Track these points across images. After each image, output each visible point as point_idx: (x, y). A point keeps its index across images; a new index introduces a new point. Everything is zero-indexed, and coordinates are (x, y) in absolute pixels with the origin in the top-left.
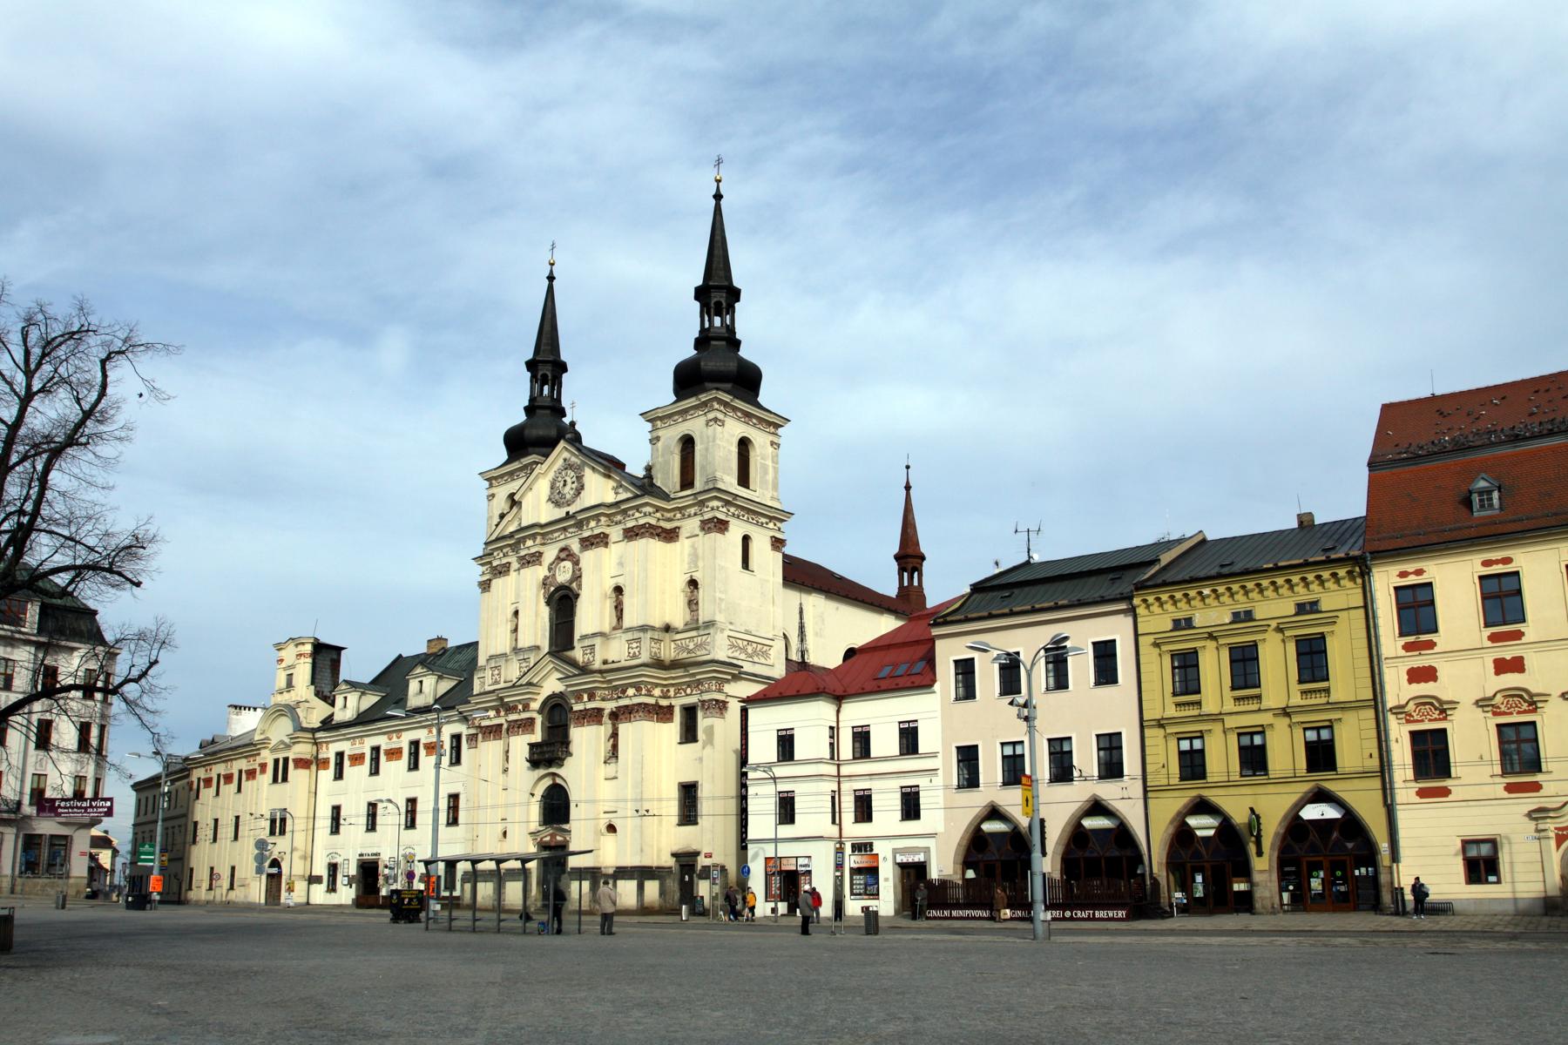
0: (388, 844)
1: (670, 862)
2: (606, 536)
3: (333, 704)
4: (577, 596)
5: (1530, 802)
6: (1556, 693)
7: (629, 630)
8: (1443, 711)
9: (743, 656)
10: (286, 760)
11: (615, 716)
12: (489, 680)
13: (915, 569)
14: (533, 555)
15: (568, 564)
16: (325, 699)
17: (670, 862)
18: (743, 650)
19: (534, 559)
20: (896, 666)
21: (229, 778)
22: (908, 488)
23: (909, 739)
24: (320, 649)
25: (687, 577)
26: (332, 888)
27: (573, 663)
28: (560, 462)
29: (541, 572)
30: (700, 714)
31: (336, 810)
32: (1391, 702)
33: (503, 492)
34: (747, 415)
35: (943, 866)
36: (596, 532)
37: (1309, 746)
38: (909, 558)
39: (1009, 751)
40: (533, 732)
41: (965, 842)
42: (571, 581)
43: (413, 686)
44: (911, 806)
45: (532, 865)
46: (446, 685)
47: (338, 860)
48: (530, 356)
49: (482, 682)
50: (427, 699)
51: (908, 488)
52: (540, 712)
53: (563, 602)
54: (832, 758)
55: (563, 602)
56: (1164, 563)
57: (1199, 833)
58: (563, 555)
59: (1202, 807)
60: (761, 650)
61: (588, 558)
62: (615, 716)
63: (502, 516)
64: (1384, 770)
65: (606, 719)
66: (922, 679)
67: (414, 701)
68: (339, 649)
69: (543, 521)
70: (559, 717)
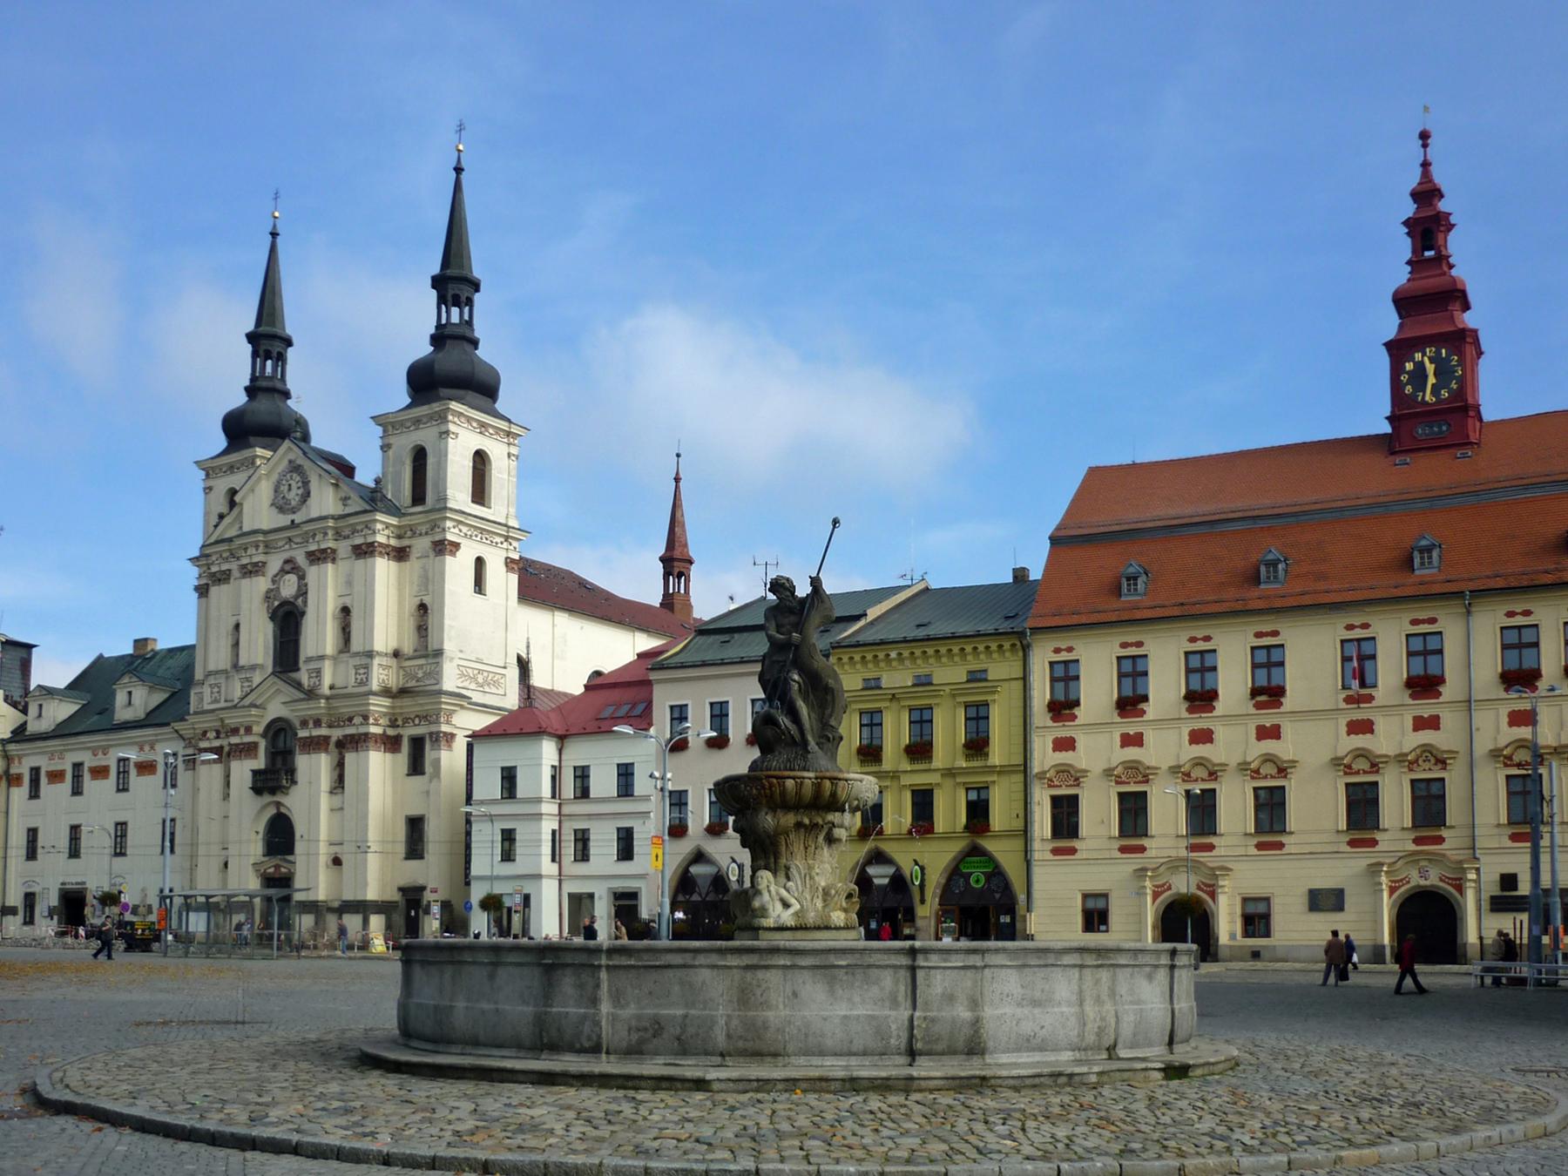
0: (93, 874)
1: (396, 897)
3: (25, 711)
4: (303, 614)
5: (1135, 861)
6: (1165, 767)
7: (357, 654)
8: (1077, 779)
9: (473, 686)
11: (342, 745)
12: (207, 698)
13: (680, 575)
14: (256, 564)
16: (14, 705)
17: (396, 897)
18: (474, 679)
20: (634, 706)
22: (677, 480)
23: (626, 774)
25: (417, 601)
26: (29, 920)
27: (298, 685)
28: (285, 463)
29: (262, 584)
31: (33, 834)
32: (1036, 768)
33: (222, 484)
34: (483, 425)
35: (654, 904)
36: (255, 560)
37: (970, 804)
38: (675, 563)
39: (973, 796)
40: (256, 757)
42: (296, 597)
43: (121, 698)
44: (626, 850)
45: (257, 901)
46: (158, 698)
47: (36, 889)
49: (202, 698)
50: (138, 711)
51: (677, 480)
52: (264, 735)
53: (288, 620)
54: (553, 797)
56: (870, 618)
57: (876, 881)
59: (878, 857)
60: (492, 681)
61: (312, 572)
62: (342, 745)
63: (221, 517)
64: (1025, 833)
65: (332, 746)
66: (642, 719)
67: (122, 714)
69: (265, 527)
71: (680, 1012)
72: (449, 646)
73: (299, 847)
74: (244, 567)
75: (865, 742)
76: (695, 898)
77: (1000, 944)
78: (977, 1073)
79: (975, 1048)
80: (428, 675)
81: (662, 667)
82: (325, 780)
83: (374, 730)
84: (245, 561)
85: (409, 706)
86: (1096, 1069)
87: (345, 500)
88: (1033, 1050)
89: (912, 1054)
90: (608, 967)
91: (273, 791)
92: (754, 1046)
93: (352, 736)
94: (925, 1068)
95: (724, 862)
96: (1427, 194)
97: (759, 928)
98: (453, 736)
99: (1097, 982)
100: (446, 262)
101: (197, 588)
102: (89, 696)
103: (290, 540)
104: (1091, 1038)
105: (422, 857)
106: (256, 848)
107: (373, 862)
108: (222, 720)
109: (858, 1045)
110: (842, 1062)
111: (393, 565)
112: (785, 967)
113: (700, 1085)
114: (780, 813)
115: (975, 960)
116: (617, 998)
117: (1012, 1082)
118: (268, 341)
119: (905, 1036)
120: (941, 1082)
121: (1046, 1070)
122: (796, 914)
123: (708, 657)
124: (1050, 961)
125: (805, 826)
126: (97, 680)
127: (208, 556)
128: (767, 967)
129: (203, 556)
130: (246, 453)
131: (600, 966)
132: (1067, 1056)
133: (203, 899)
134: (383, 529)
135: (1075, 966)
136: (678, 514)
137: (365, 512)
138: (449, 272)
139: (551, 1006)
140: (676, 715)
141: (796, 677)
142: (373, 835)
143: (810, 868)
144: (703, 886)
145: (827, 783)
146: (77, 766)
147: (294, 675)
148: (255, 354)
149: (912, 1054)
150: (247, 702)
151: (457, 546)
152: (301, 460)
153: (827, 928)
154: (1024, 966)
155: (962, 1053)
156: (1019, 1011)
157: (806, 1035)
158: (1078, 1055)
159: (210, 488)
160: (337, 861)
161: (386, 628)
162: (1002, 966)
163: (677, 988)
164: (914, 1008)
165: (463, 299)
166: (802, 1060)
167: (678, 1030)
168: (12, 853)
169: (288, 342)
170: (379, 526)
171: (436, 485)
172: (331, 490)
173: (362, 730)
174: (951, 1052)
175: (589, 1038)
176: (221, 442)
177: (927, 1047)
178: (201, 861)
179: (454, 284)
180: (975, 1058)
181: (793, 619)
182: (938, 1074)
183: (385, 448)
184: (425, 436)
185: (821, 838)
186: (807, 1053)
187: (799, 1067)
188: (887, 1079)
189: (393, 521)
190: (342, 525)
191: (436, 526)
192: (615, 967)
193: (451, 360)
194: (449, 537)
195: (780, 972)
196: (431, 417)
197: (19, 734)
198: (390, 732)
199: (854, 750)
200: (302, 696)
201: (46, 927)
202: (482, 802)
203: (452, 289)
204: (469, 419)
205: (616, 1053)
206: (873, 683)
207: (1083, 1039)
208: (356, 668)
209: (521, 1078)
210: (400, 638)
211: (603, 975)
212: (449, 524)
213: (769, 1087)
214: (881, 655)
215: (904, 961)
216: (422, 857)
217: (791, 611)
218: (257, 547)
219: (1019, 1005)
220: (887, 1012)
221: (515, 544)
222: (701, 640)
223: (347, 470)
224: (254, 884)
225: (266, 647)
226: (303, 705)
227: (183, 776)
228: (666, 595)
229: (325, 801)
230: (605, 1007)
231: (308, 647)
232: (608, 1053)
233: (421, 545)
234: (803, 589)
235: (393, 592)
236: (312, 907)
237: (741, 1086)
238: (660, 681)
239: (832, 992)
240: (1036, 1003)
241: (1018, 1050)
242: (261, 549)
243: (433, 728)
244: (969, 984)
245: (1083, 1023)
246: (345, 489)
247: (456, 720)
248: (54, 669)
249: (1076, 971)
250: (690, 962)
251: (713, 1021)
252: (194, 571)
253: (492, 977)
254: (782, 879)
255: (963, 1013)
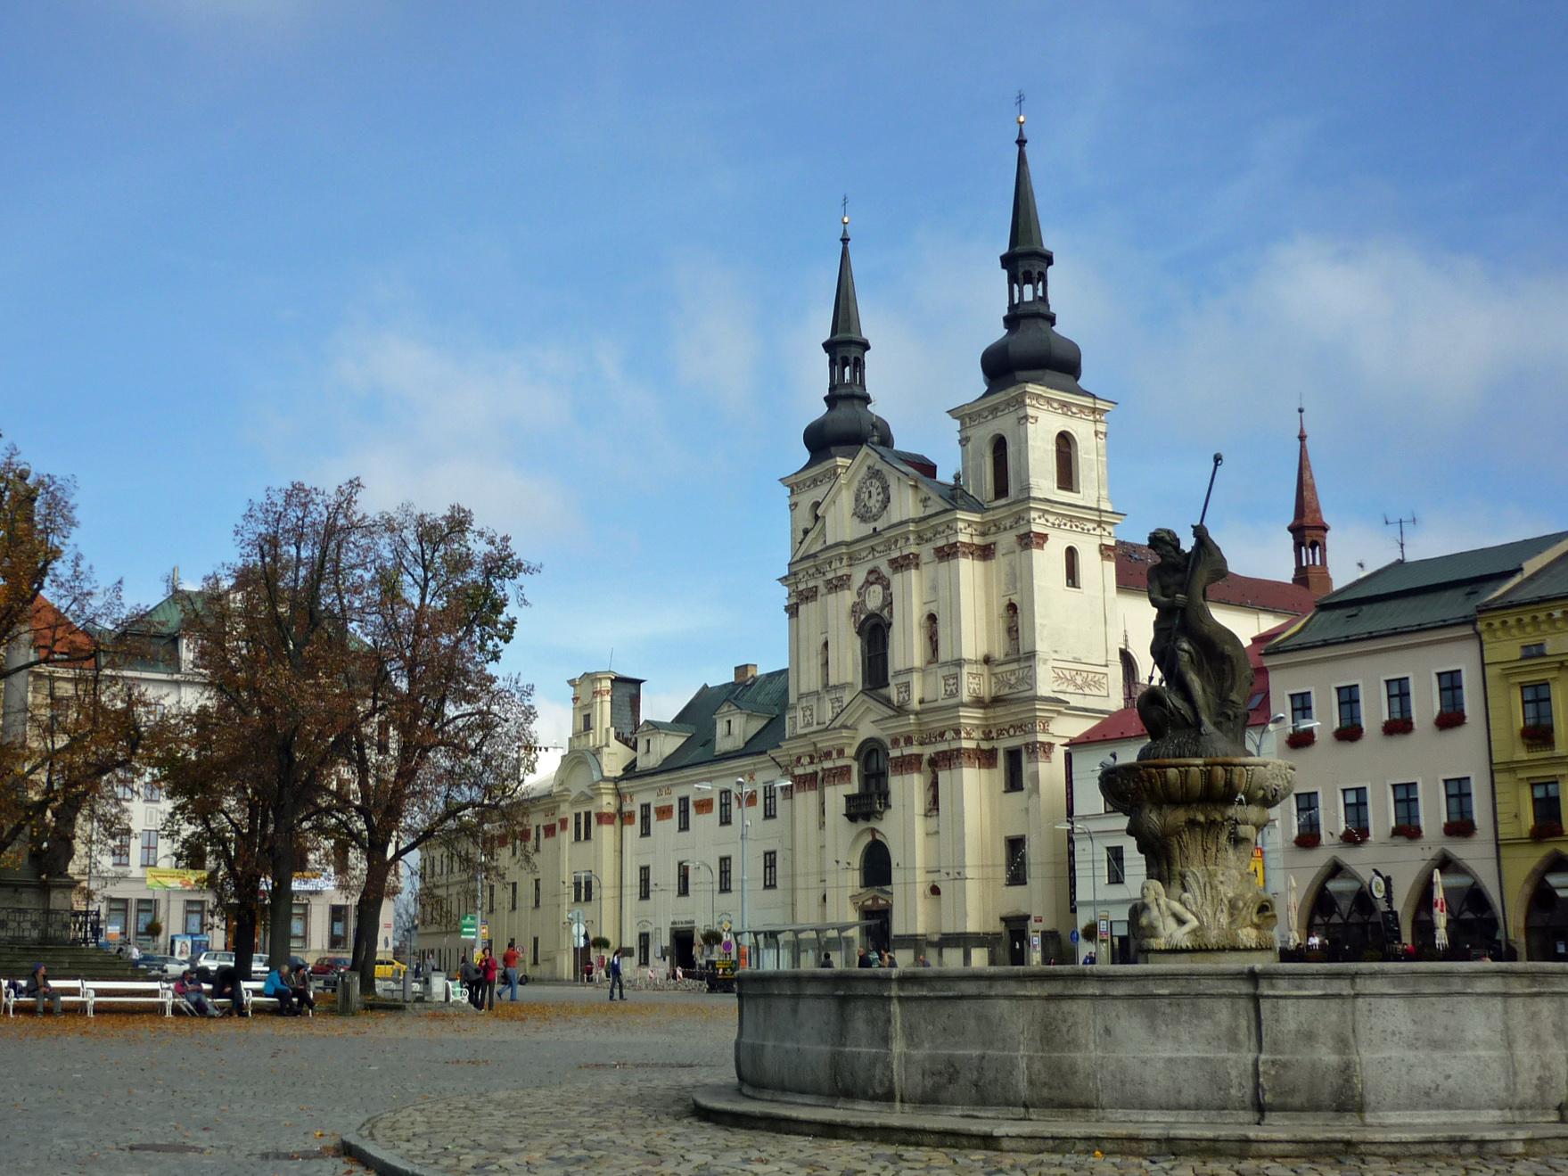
0: (701, 912)
1: (999, 927)
2: (917, 556)
3: (635, 748)
4: (890, 624)
7: (945, 664)
10: (588, 815)
12: (800, 722)
13: (1313, 545)
14: (840, 578)
15: (878, 588)
16: (625, 742)
17: (999, 927)
18: (1072, 681)
19: (838, 584)
21: (704, 806)
22: (1302, 438)
24: (618, 681)
26: (644, 962)
27: (887, 702)
29: (848, 598)
30: (1024, 758)
31: (645, 871)
33: (806, 499)
34: (1064, 405)
38: (1307, 532)
39: (1540, 793)
40: (849, 781)
41: (1308, 904)
42: (882, 609)
43: (721, 728)
46: (756, 725)
47: (650, 929)
48: (827, 336)
49: (796, 722)
50: (736, 742)
51: (1302, 438)
52: (856, 758)
53: (875, 632)
55: (875, 632)
58: (872, 578)
60: (1094, 682)
61: (897, 580)
63: (806, 532)
67: (723, 744)
68: (638, 682)
69: (848, 539)
70: (876, 766)
71: (975, 1052)
72: (1041, 647)
73: (896, 875)
74: (830, 581)
75: (1531, 722)
76: (1336, 919)
77: (1376, 966)
78: (1338, 1135)
79: (1348, 1102)
80: (1020, 680)
81: (1277, 651)
82: (919, 802)
83: (966, 744)
84: (830, 576)
85: (1002, 715)
86: (1520, 1135)
87: (925, 501)
88: (1438, 1107)
89: (1260, 1108)
90: (900, 998)
91: (867, 817)
92: (1062, 1097)
93: (944, 752)
94: (1279, 1128)
95: (1366, 875)
96: (1302, 430)
97: (1149, 951)
98: (1051, 745)
99: (1534, 1016)
100: (1014, 241)
101: (787, 609)
102: (694, 729)
103: (873, 549)
104: (1527, 1093)
105: (1025, 883)
106: (854, 879)
107: (972, 890)
108: (815, 744)
109: (1188, 1096)
110: (1168, 1117)
111: (978, 564)
112: (1093, 996)
113: (988, 1142)
114: (1166, 810)
115: (1343, 987)
116: (911, 1036)
117: (1390, 1149)
118: (846, 349)
119: (1249, 1085)
120: (1289, 1147)
121: (1440, 1135)
122: (1194, 931)
123: (1329, 635)
124: (1455, 988)
125: (1199, 824)
126: (699, 714)
127: (795, 574)
128: (1073, 997)
129: (793, 574)
130: (828, 464)
131: (890, 998)
132: (1493, 1115)
133: (813, 935)
134: (966, 527)
135: (1494, 994)
136: (1306, 476)
137: (946, 511)
138: (1018, 249)
139: (844, 1045)
140: (1298, 705)
141: (1185, 646)
142: (971, 858)
143: (1211, 875)
144: (1344, 905)
145: (1219, 771)
146: (646, 807)
147: (883, 691)
148: (832, 363)
149: (1260, 1108)
150: (837, 723)
151: (1044, 537)
152: (880, 465)
153: (1235, 949)
154: (1415, 995)
155: (1328, 1109)
156: (1410, 1055)
157: (1123, 1083)
158: (1508, 1115)
159: (796, 504)
160: (935, 891)
161: (974, 634)
162: (1382, 995)
163: (972, 1023)
164: (1260, 1049)
165: (1035, 275)
166: (1119, 1114)
167: (975, 1076)
168: (627, 891)
169: (865, 346)
170: (961, 525)
171: (1018, 474)
172: (910, 492)
173: (954, 745)
174: (1315, 1107)
175: (881, 1083)
176: (805, 456)
177: (1278, 1101)
178: (800, 895)
179: (1025, 261)
180: (1348, 1116)
181: (1178, 577)
182: (1283, 1136)
183: (964, 441)
184: (1004, 424)
185: (1223, 839)
186: (1126, 1104)
187: (1116, 1123)
188: (1215, 1140)
189: (976, 518)
190: (924, 527)
191: (1020, 518)
192: (908, 999)
193: (1029, 338)
194: (1035, 528)
195: (1089, 1003)
196: (1008, 404)
197: (630, 771)
198: (985, 746)
199: (1517, 733)
200: (892, 713)
201: (660, 968)
202: (1084, 818)
203: (1023, 267)
204: (1049, 401)
205: (911, 1101)
206: (1534, 650)
207: (1514, 1093)
208: (945, 678)
209: (805, 1128)
210: (990, 641)
211: (895, 1008)
212: (1034, 514)
213: (1068, 1146)
214: (1542, 616)
215: (1245, 988)
216: (1025, 883)
217: (1176, 568)
218: (841, 560)
219: (1411, 1046)
220: (1224, 1054)
221: (1109, 529)
222: (1323, 616)
223: (928, 469)
224: (853, 916)
225: (855, 665)
226: (891, 724)
227: (781, 805)
228: (1300, 569)
229: (919, 826)
230: (898, 1047)
231: (896, 661)
232: (902, 1101)
233: (1006, 540)
234: (1187, 544)
235: (980, 593)
236: (912, 942)
237: (1034, 1144)
238: (1276, 667)
239: (1152, 1028)
240: (1436, 1044)
241: (1414, 1106)
242: (845, 562)
243: (1029, 739)
244: (1334, 1017)
245: (1512, 1072)
246: (925, 490)
247: (1053, 728)
248: (661, 704)
249: (1498, 1003)
250: (985, 991)
251: (1012, 1063)
252: (785, 591)
253: (795, 1011)
254: (1176, 890)
255: (1327, 1056)
